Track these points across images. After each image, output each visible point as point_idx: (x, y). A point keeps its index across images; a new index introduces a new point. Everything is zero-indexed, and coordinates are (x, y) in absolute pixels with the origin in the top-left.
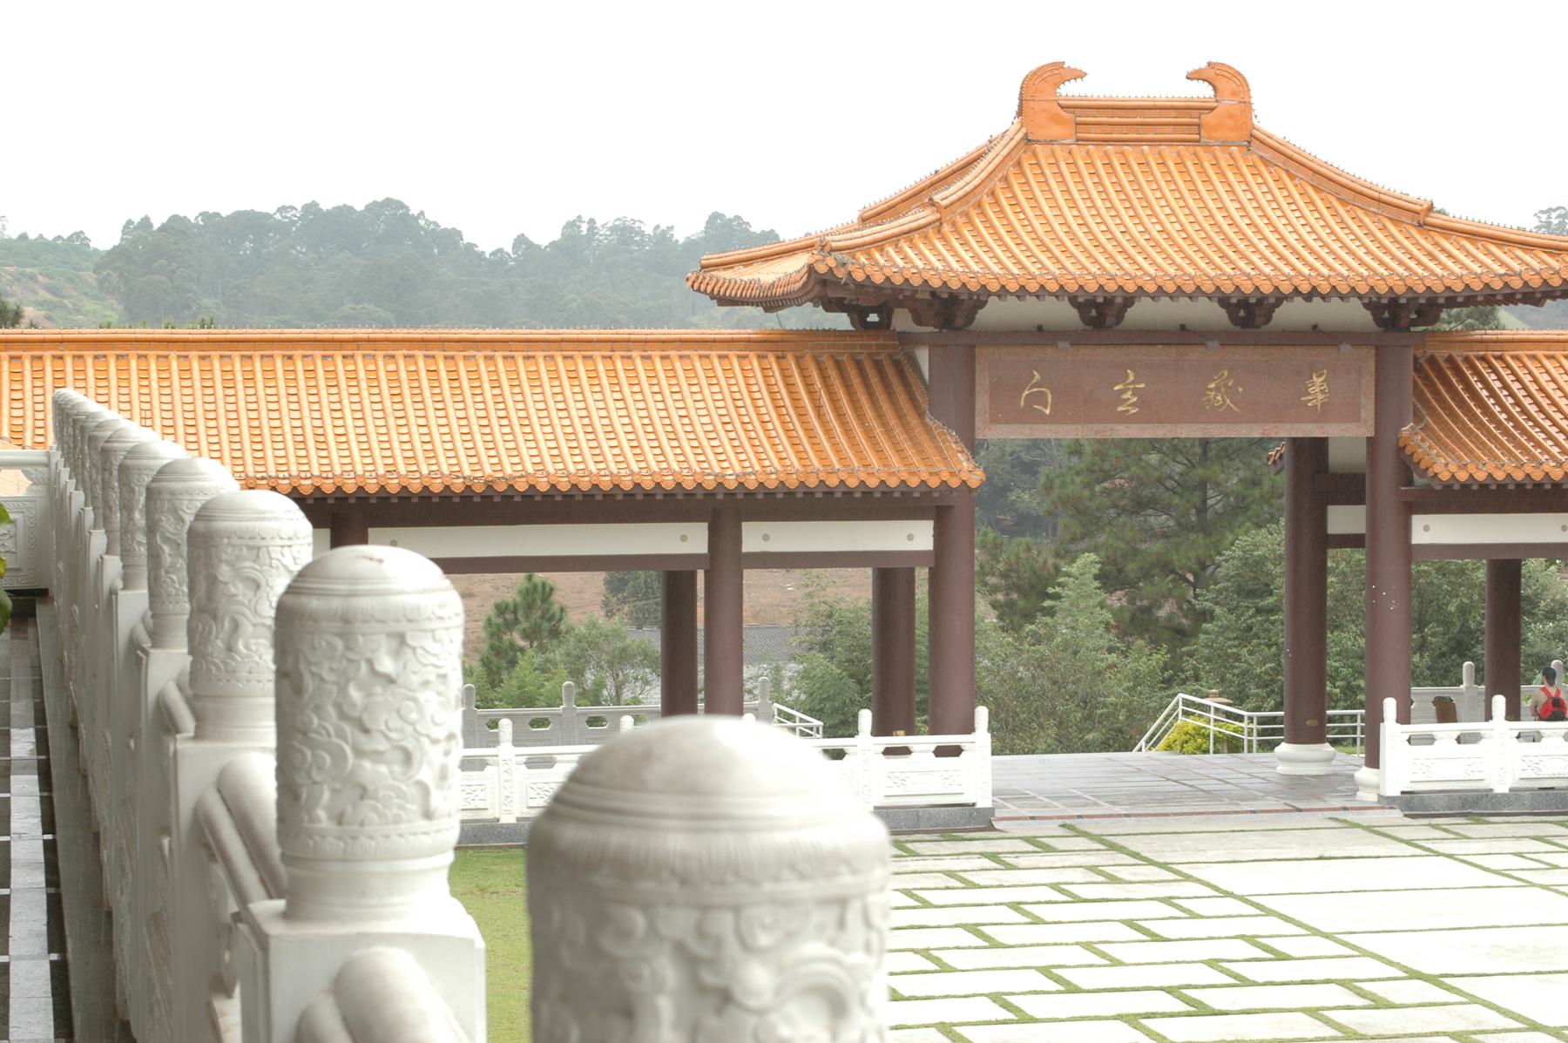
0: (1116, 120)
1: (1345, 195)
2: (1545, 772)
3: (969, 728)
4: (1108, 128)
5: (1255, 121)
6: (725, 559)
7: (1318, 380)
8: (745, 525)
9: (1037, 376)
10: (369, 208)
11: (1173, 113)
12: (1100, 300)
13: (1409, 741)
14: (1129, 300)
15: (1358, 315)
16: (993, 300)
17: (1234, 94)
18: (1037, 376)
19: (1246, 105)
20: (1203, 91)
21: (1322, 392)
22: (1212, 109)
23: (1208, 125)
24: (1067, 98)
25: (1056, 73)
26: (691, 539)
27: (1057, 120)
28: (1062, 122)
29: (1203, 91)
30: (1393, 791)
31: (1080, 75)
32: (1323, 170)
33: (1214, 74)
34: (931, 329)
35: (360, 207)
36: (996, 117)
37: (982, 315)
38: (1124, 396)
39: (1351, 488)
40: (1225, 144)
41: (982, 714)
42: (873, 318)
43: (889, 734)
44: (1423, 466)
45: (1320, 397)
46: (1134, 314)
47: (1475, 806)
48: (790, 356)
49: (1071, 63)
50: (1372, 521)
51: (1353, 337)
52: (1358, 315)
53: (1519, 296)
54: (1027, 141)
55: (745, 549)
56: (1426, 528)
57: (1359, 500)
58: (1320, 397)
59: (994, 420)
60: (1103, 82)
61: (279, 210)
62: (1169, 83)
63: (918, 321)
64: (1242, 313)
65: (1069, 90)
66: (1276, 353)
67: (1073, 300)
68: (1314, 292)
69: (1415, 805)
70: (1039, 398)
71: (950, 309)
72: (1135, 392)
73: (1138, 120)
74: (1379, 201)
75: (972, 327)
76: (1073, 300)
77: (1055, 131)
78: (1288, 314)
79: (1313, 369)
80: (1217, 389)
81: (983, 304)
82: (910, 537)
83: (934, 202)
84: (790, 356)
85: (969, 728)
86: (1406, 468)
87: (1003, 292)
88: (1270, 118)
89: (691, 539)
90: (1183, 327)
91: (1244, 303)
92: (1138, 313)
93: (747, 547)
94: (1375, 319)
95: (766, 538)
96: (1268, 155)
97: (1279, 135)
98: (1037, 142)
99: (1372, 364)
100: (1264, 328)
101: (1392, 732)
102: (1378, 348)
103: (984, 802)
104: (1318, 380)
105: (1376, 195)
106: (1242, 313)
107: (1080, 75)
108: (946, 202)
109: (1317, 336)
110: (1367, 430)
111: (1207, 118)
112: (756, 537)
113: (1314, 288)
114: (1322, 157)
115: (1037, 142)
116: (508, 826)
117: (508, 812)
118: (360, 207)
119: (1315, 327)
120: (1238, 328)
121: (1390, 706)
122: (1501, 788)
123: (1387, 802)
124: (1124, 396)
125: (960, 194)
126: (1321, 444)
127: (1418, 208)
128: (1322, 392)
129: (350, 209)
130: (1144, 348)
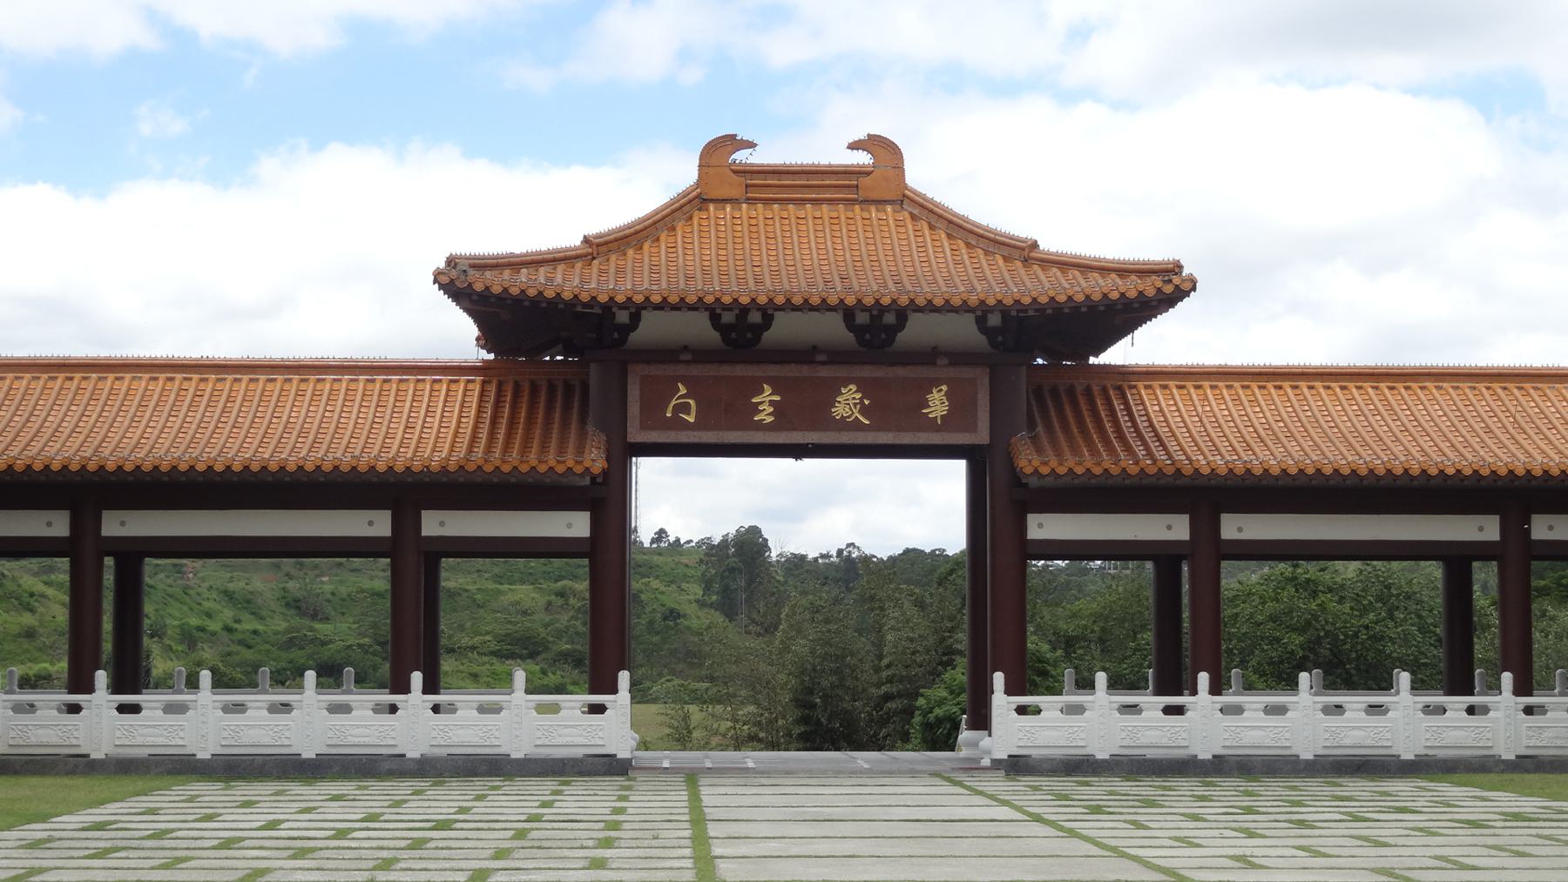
3: (613, 690)
8: (105, 514)
13: (1445, 711)
20: (863, 158)
22: (869, 173)
25: (730, 143)
28: (731, 180)
29: (863, 158)
30: (1002, 755)
31: (751, 145)
33: (874, 143)
36: (683, 174)
41: (624, 678)
43: (1530, 694)
47: (1079, 767)
49: (743, 135)
56: (1040, 526)
59: (644, 427)
65: (741, 156)
69: (1016, 766)
70: (685, 408)
72: (772, 403)
82: (1551, 528)
83: (598, 248)
85: (613, 690)
88: (920, 176)
89: (1174, 528)
95: (371, 523)
99: (986, 381)
101: (1002, 703)
103: (623, 754)
107: (751, 145)
109: (928, 356)
111: (864, 181)
112: (1236, 527)
115: (712, 201)
116: (202, 761)
117: (204, 749)
119: (935, 348)
121: (999, 679)
123: (997, 764)
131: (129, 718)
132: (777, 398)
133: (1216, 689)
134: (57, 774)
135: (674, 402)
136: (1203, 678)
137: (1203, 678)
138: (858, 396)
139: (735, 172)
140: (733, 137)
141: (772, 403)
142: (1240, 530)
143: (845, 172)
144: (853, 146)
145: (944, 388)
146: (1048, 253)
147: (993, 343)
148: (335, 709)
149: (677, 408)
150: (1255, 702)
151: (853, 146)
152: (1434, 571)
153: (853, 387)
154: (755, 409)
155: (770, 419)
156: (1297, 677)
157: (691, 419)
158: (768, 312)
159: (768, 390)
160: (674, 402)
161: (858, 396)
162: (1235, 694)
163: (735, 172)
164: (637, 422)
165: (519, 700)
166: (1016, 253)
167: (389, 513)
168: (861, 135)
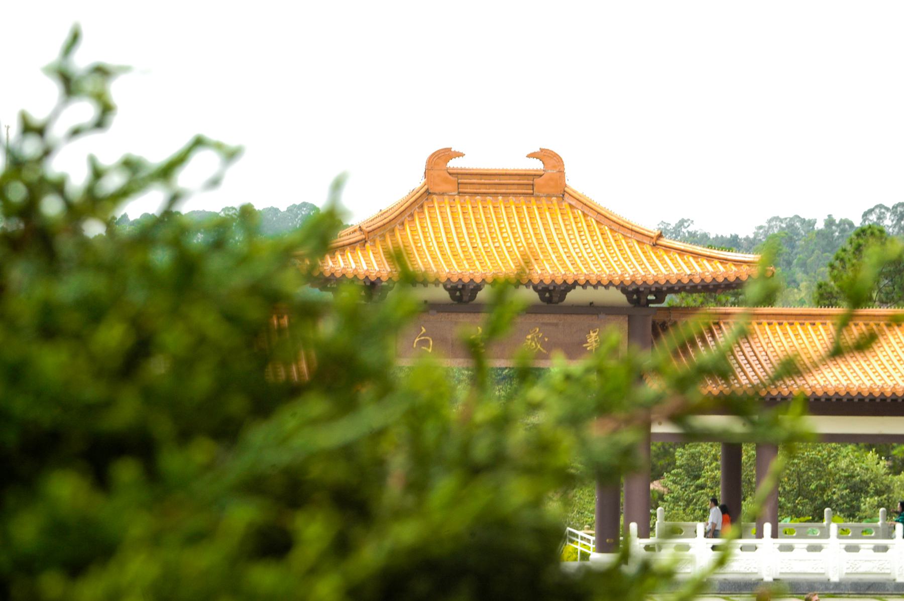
0: (483, 181)
1: (615, 227)
2: (861, 570)
4: (478, 186)
5: (567, 182)
7: (593, 335)
9: (424, 330)
10: (290, 210)
11: (518, 177)
12: (460, 287)
14: (478, 288)
15: (617, 297)
17: (554, 167)
18: (424, 330)
19: (562, 172)
21: (596, 341)
22: (541, 176)
23: (539, 185)
24: (453, 169)
25: (446, 154)
27: (446, 181)
28: (449, 183)
29: (536, 165)
31: (460, 155)
32: (603, 212)
33: (544, 155)
35: (283, 209)
40: (549, 196)
45: (594, 344)
46: (573, 296)
51: (610, 310)
52: (617, 297)
53: (699, 287)
54: (428, 193)
58: (594, 344)
60: (473, 160)
61: (223, 210)
62: (518, 161)
64: (635, 297)
65: (454, 164)
66: (570, 319)
67: (535, 288)
68: (599, 283)
73: (496, 181)
74: (632, 230)
77: (444, 187)
78: (573, 296)
79: (592, 328)
80: (533, 339)
87: (576, 283)
88: (575, 181)
91: (637, 291)
96: (573, 203)
97: (580, 192)
98: (434, 194)
100: (560, 304)
102: (629, 316)
104: (593, 335)
105: (630, 227)
106: (547, 295)
107: (460, 155)
108: (369, 229)
109: (592, 309)
111: (537, 181)
113: (587, 281)
114: (603, 205)
115: (434, 194)
118: (283, 209)
119: (591, 303)
120: (545, 304)
122: (835, 578)
125: (379, 224)
127: (652, 235)
128: (596, 341)
129: (276, 210)
130: (533, 316)
131: (787, 555)
133: (775, 535)
134: (865, 584)
135: (417, 339)
136: (767, 527)
137: (767, 527)
139: (450, 174)
143: (525, 175)
144: (529, 156)
147: (630, 300)
148: (850, 549)
150: (800, 544)
151: (529, 156)
152: (716, 449)
158: (568, 287)
162: (852, 537)
163: (450, 174)
165: (834, 544)
166: (646, 240)
168: (529, 152)
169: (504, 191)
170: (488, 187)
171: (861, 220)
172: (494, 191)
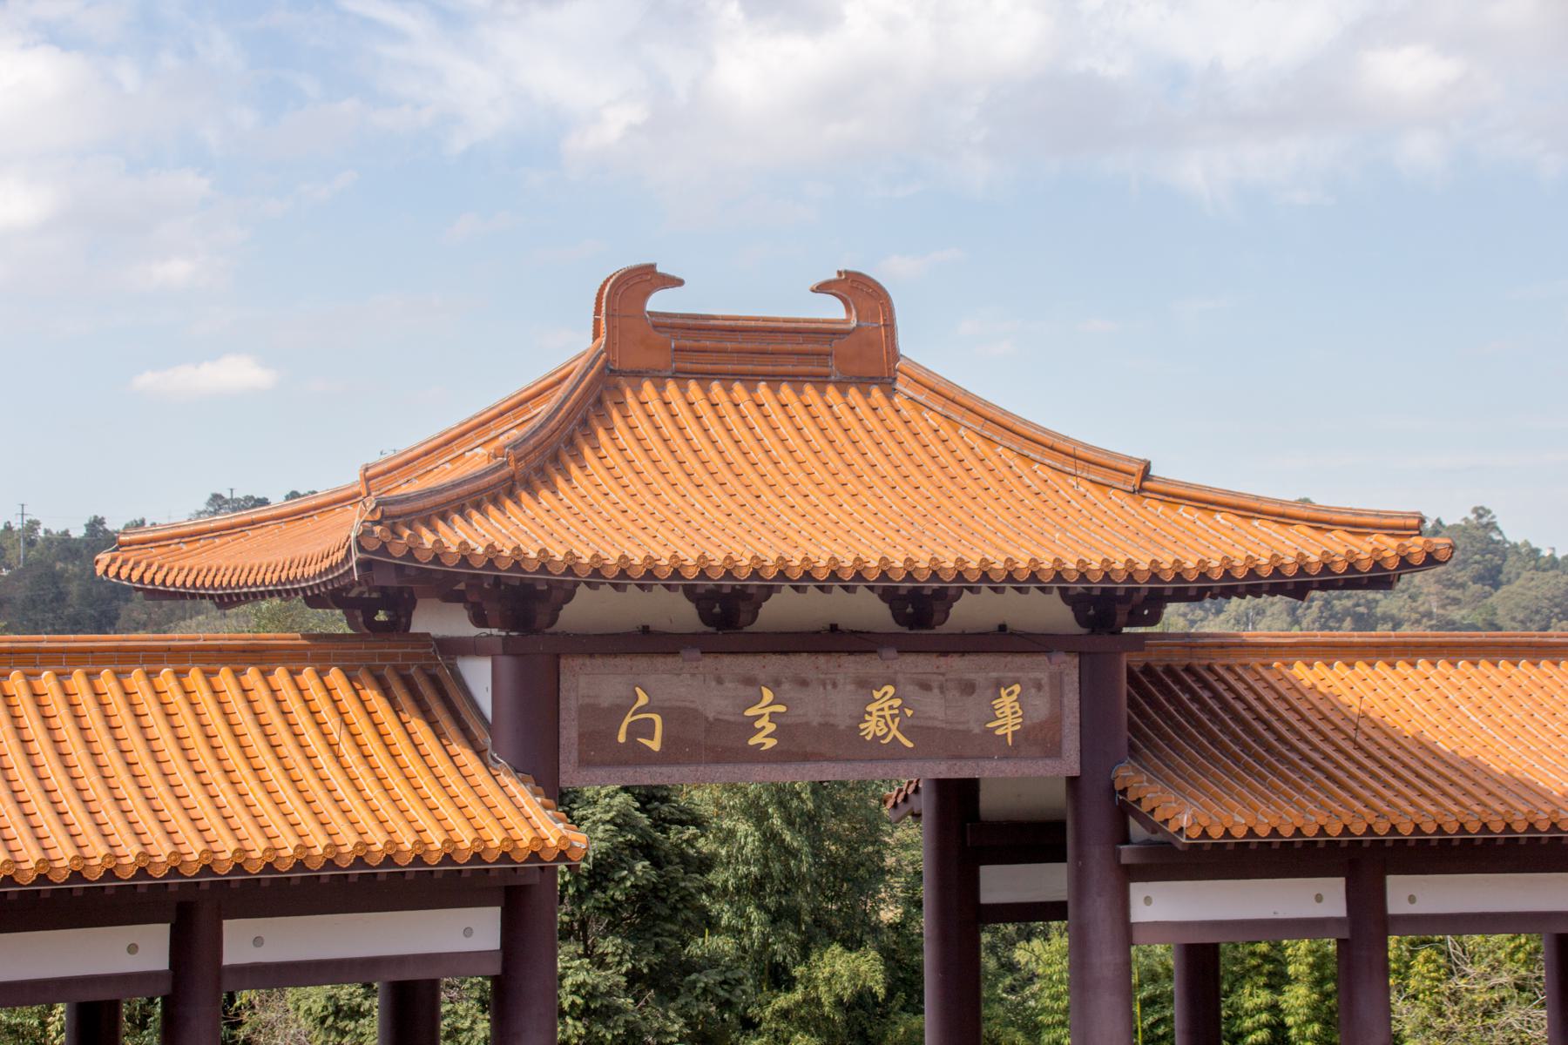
6: (1366, 928)
15: (1055, 614)
16: (582, 590)
19: (890, 326)
20: (832, 310)
23: (845, 351)
25: (643, 279)
26: (144, 949)
29: (832, 310)
33: (855, 288)
34: (495, 631)
36: (567, 340)
37: (957, 609)
38: (758, 725)
39: (1036, 839)
42: (381, 616)
44: (1145, 808)
48: (106, 672)
50: (1079, 882)
52: (1055, 614)
53: (1265, 588)
55: (227, 960)
57: (1060, 857)
60: (706, 291)
63: (479, 620)
65: (659, 302)
67: (690, 591)
71: (523, 604)
72: (773, 717)
75: (557, 627)
76: (690, 591)
78: (967, 612)
81: (570, 596)
82: (258, 942)
84: (106, 672)
86: (1123, 810)
87: (597, 574)
88: (920, 343)
90: (834, 628)
91: (916, 595)
92: (967, 612)
93: (230, 958)
94: (894, 616)
95: (468, 932)
98: (621, 373)
109: (1003, 641)
110: (1070, 763)
115: (621, 373)
119: (1002, 628)
120: (905, 630)
124: (758, 725)
126: (968, 789)
132: (781, 709)
138: (897, 702)
140: (650, 269)
141: (773, 717)
142: (1412, 899)
144: (823, 288)
145: (1017, 688)
146: (1166, 481)
149: (633, 731)
151: (823, 288)
153: (890, 689)
154: (750, 728)
155: (771, 743)
156: (221, 925)
157: (655, 745)
159: (768, 695)
160: (628, 719)
161: (897, 702)
164: (574, 756)
167: (496, 912)
169: (770, 369)
170: (800, 338)
171: (121, 528)
172: (750, 368)
